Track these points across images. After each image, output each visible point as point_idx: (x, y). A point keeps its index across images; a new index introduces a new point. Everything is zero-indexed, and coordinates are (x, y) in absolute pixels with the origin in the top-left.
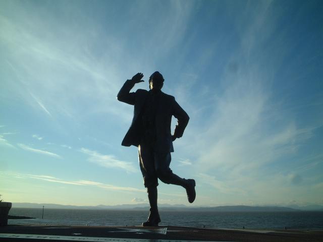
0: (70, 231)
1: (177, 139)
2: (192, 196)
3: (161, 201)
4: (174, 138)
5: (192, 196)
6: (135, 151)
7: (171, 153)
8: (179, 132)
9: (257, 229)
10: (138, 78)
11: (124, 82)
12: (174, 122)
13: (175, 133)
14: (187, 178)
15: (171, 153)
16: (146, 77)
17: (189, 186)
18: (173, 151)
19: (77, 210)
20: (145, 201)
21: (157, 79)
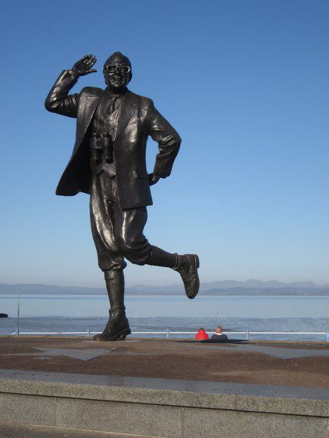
0: (84, 319)
1: (161, 180)
2: (192, 288)
3: (133, 309)
4: (152, 180)
5: (192, 288)
6: (82, 198)
7: (148, 208)
8: (164, 169)
9: (270, 331)
10: (83, 67)
11: (62, 173)
12: (152, 149)
13: (156, 167)
14: (181, 253)
15: (148, 208)
16: (99, 66)
17: (187, 266)
18: (151, 203)
19: (30, 338)
20: (101, 308)
21: (120, 69)
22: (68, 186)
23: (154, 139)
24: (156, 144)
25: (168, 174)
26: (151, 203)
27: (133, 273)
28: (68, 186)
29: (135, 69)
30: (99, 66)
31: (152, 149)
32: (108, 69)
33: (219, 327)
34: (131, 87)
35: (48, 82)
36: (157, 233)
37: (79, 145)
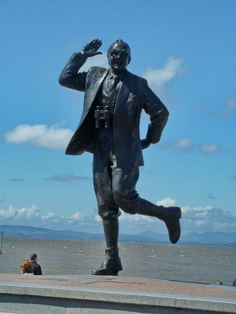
2: (174, 234)
4: (146, 144)
5: (174, 234)
6: (88, 157)
7: (140, 168)
8: (154, 135)
10: (93, 47)
12: (145, 120)
15: (140, 168)
17: (171, 217)
18: (142, 164)
22: (74, 148)
23: (147, 112)
24: (149, 116)
25: (165, 113)
26: (121, 269)
27: (123, 217)
28: (74, 148)
29: (133, 54)
30: (104, 49)
31: (145, 120)
32: (112, 53)
33: (215, 197)
34: (130, 68)
35: (62, 63)
36: (144, 189)
37: (84, 117)
